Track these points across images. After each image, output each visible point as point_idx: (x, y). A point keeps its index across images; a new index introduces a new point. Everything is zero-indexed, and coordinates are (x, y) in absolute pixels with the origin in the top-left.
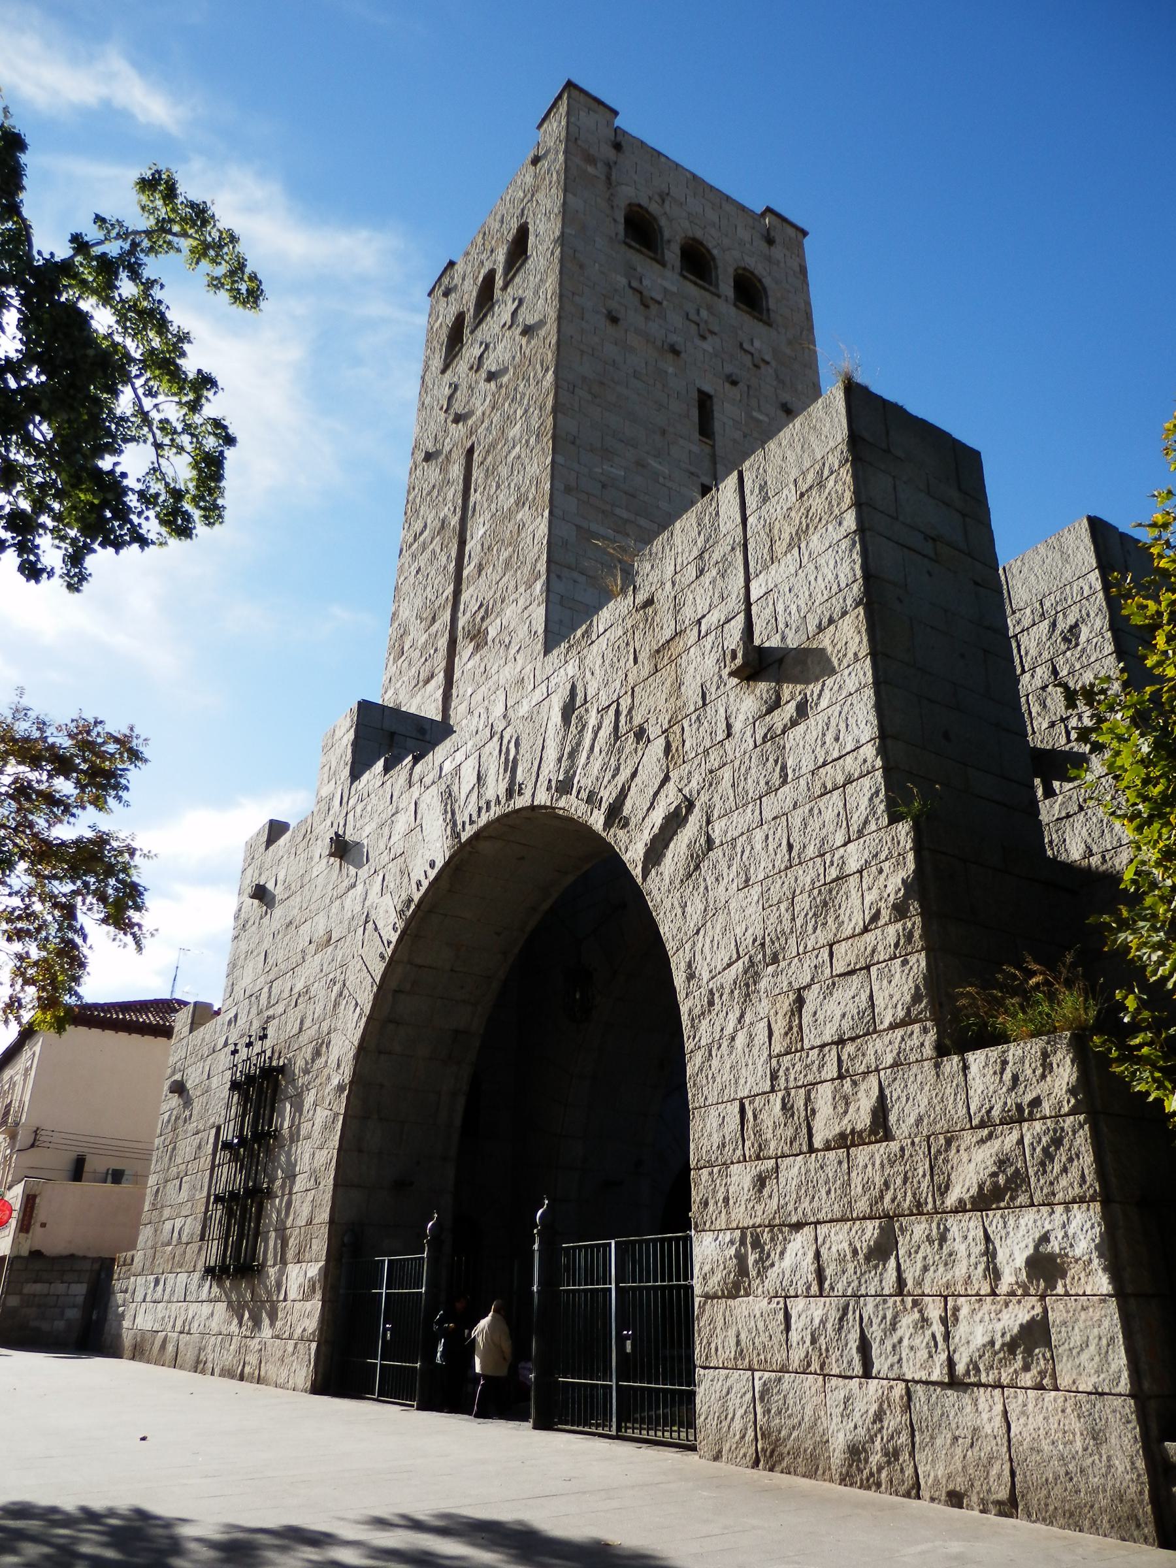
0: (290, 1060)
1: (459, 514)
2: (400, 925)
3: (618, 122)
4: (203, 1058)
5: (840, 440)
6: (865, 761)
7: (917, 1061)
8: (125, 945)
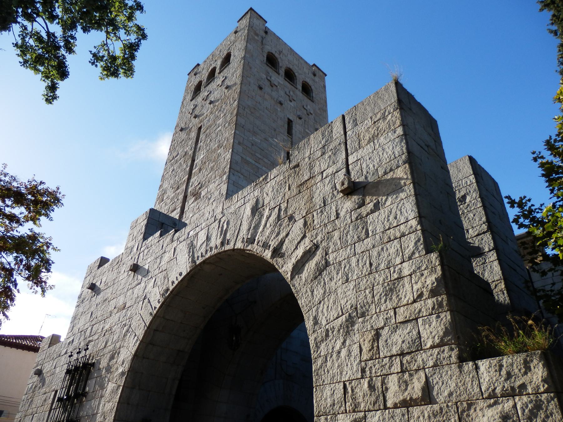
0: (98, 360)
1: (193, 150)
2: (162, 300)
3: (267, 25)
4: (53, 359)
5: (393, 101)
6: (411, 227)
7: (447, 364)
8: (36, 292)
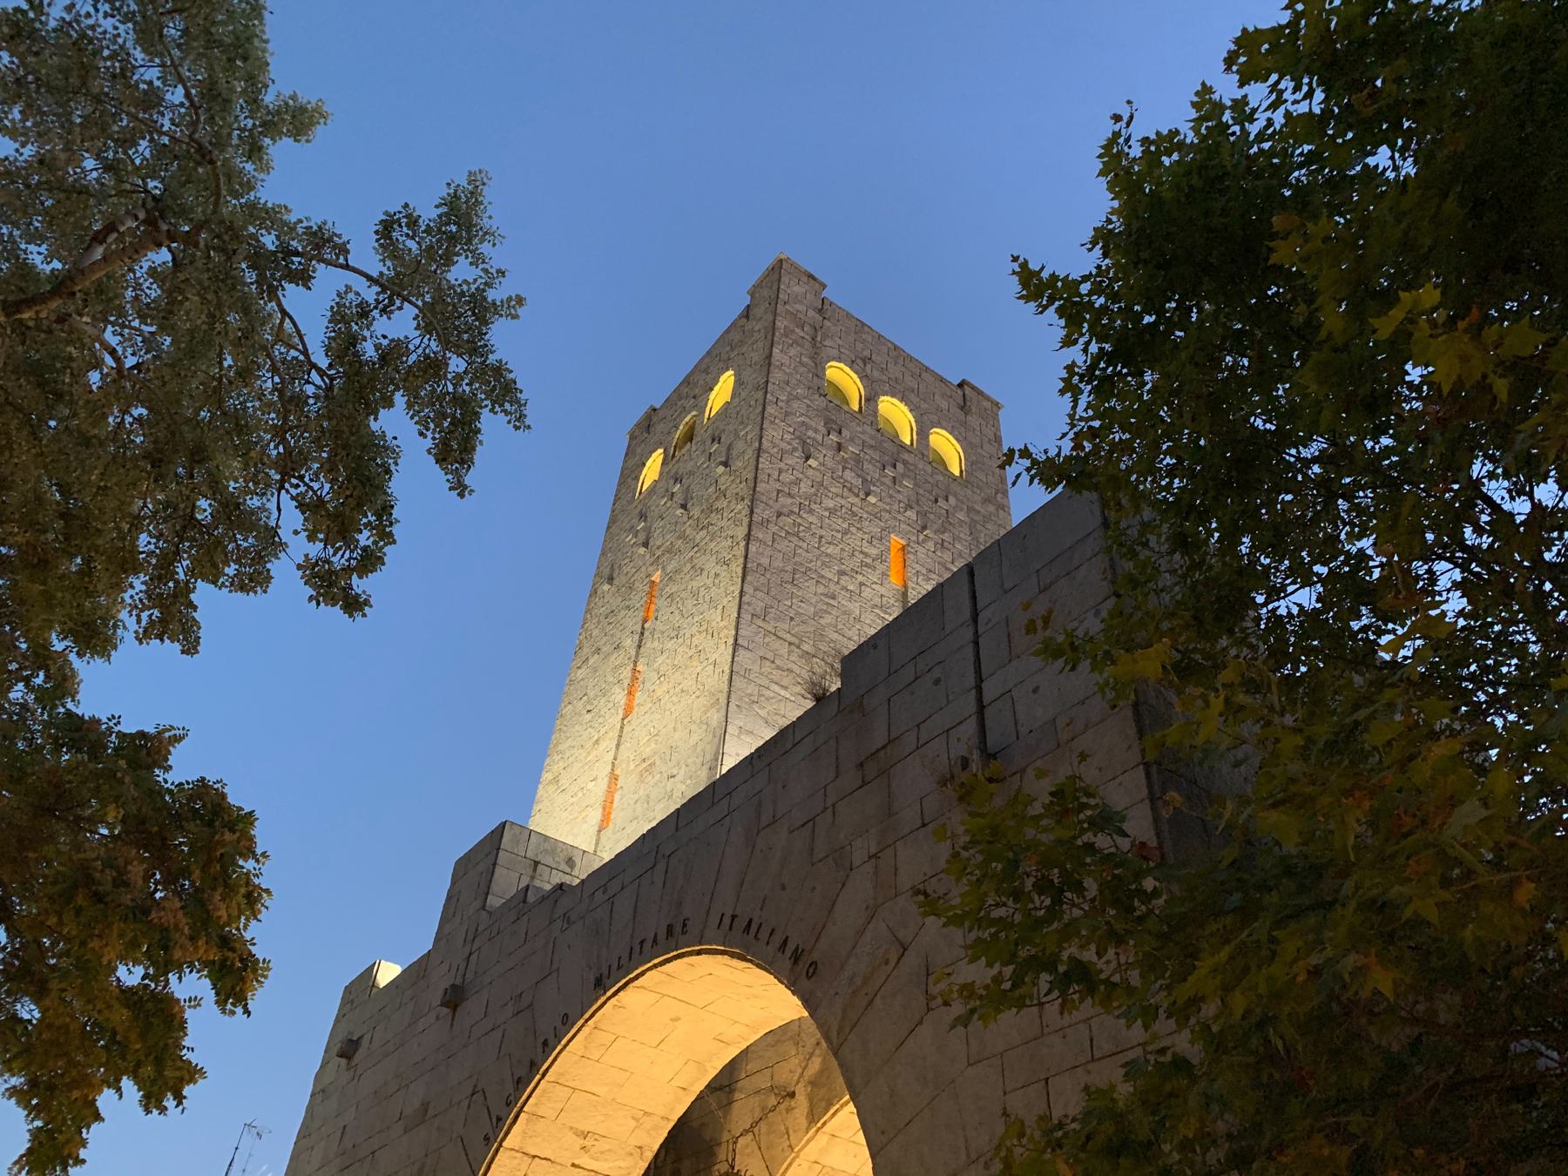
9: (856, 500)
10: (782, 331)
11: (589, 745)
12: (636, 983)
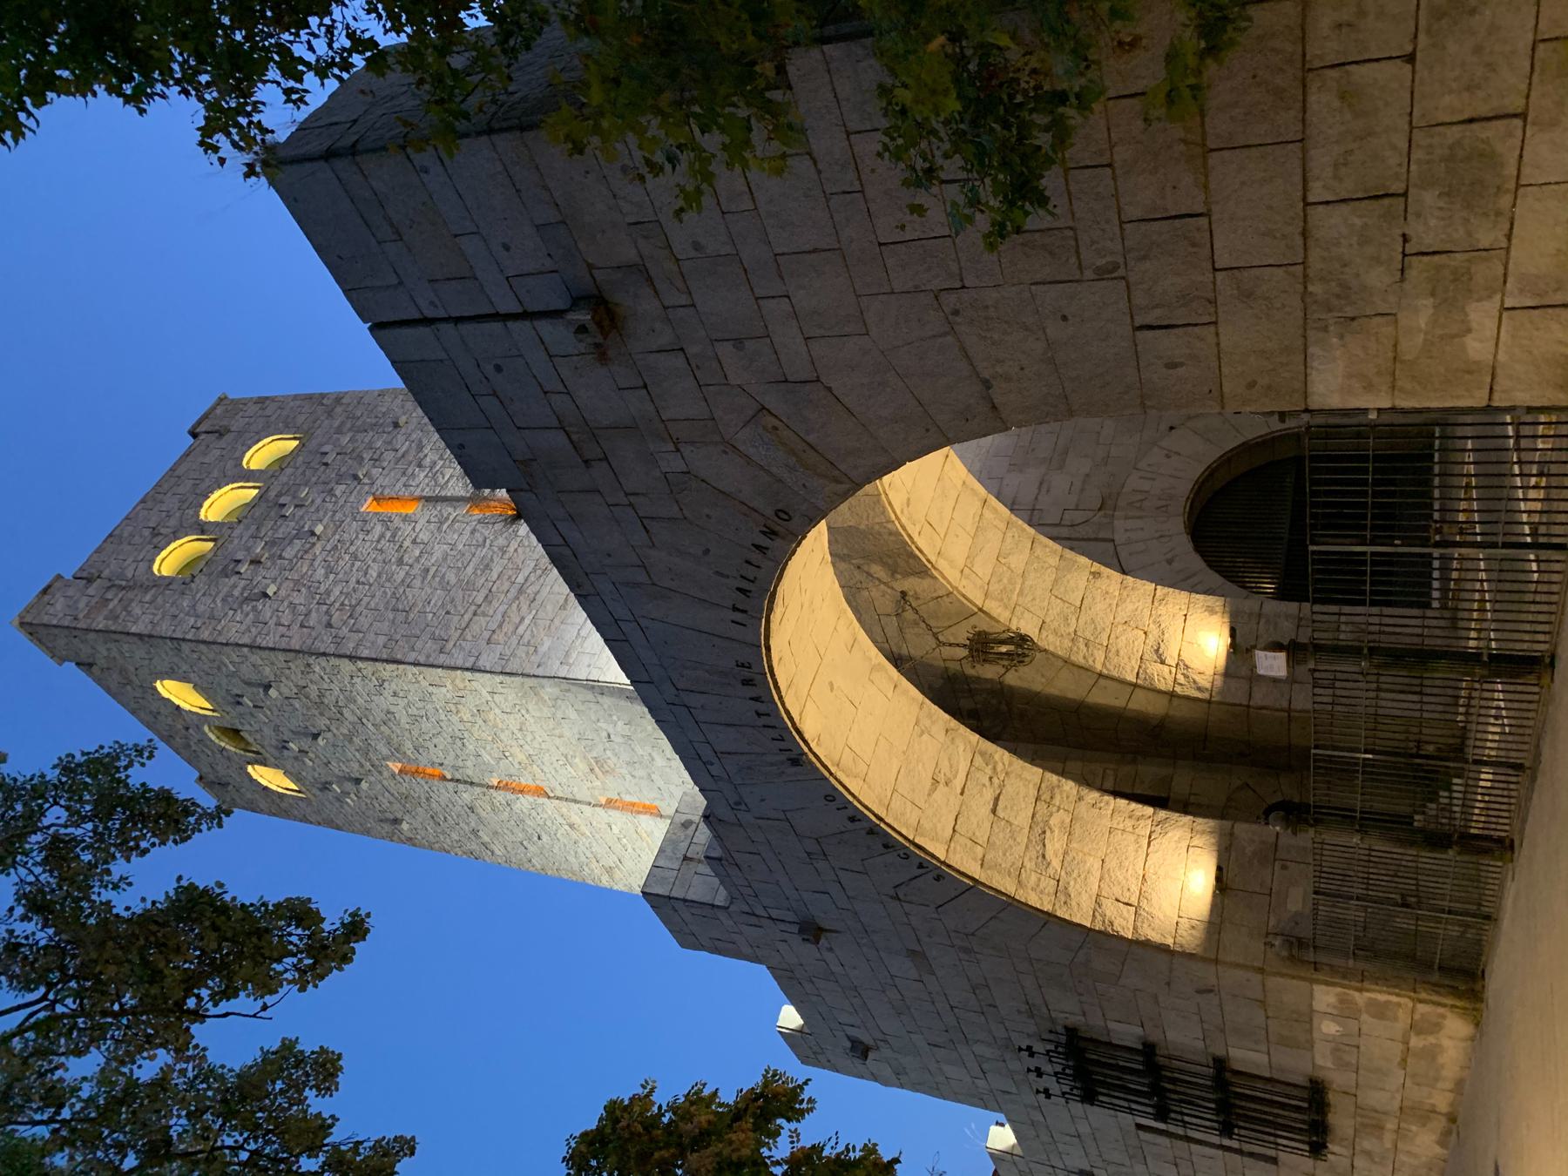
3: (68, 576)
9: (318, 549)
10: (110, 622)
11: (574, 835)
12: (796, 719)
